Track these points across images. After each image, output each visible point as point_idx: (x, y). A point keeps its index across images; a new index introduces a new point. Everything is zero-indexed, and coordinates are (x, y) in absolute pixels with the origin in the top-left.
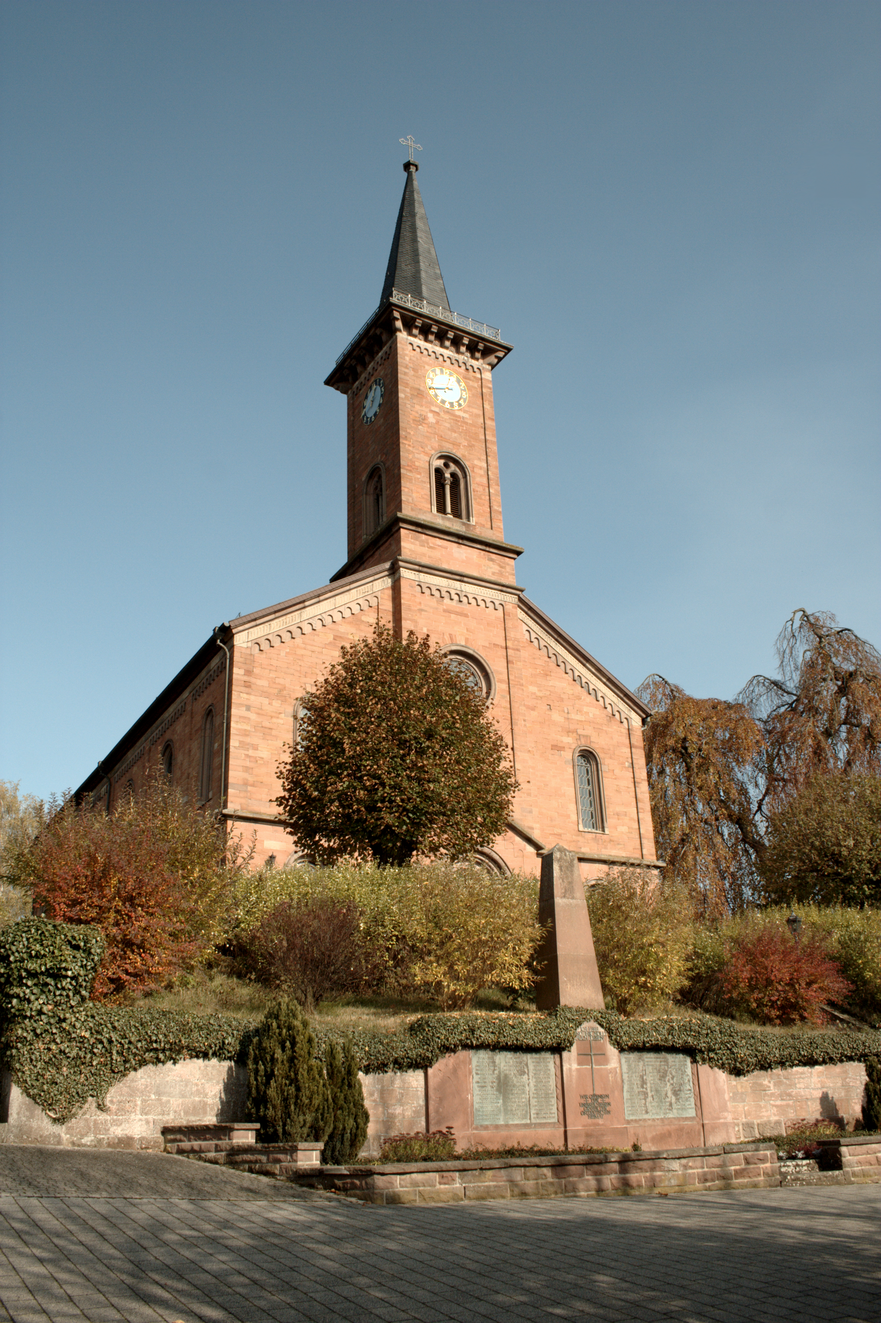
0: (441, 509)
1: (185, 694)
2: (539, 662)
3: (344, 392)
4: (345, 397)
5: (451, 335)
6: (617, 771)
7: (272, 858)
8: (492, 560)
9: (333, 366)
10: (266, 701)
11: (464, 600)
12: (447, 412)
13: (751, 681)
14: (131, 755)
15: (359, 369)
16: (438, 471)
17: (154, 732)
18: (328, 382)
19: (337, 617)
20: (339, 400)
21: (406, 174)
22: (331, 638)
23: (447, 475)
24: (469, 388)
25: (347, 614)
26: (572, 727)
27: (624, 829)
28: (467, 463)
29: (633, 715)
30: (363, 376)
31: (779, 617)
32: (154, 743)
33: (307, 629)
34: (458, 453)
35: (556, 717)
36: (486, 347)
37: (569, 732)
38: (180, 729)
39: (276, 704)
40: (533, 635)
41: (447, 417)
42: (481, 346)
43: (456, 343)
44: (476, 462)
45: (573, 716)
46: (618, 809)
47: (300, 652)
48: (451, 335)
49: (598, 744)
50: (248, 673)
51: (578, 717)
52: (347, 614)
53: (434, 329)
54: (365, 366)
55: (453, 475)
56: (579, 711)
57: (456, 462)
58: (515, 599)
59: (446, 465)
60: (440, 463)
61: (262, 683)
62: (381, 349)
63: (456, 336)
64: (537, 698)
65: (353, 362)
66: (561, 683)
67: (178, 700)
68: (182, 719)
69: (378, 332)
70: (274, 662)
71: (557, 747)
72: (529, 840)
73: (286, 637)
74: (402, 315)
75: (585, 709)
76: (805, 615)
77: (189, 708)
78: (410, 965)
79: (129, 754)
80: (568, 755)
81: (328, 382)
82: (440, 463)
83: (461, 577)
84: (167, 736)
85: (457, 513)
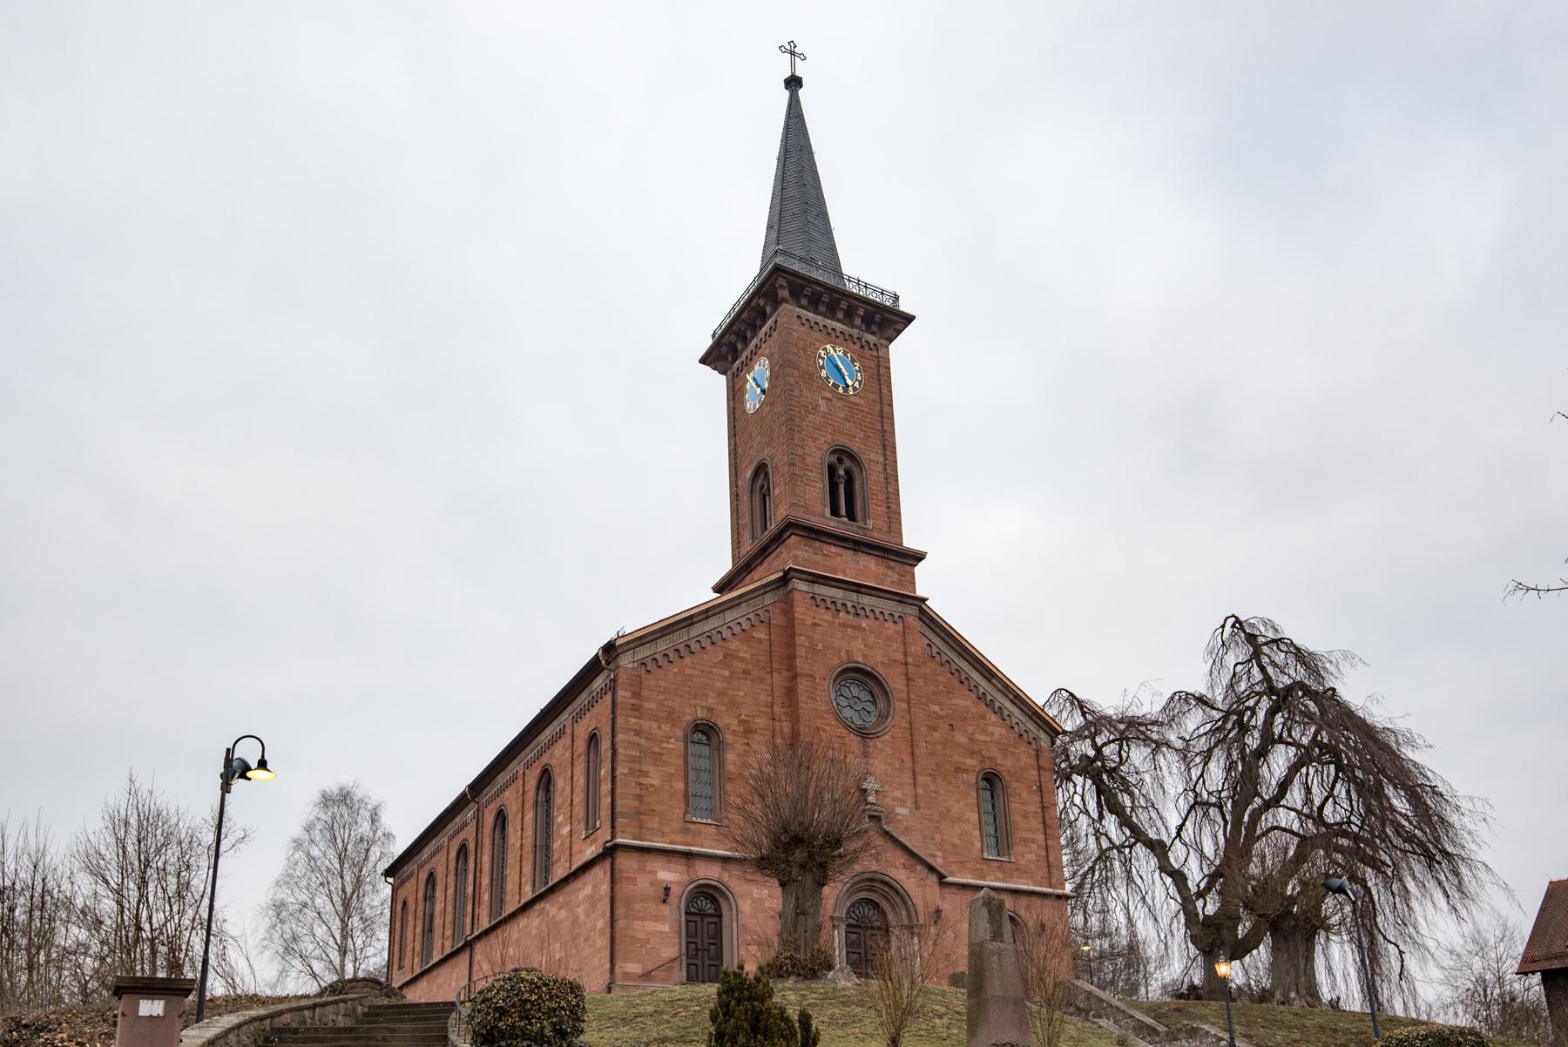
0: (835, 512)
1: (564, 716)
2: (940, 678)
3: (723, 372)
4: (724, 378)
5: (844, 305)
6: (1024, 795)
7: (667, 889)
8: (890, 568)
9: (709, 342)
10: (655, 725)
11: (862, 613)
12: (840, 398)
13: (1172, 698)
14: (501, 779)
15: (739, 346)
16: (832, 470)
17: (527, 754)
18: (703, 361)
19: (726, 633)
20: (717, 383)
21: (787, 93)
22: (721, 657)
23: (842, 472)
24: (864, 368)
25: (737, 630)
26: (976, 748)
27: (1032, 857)
28: (863, 458)
29: (1043, 735)
30: (745, 354)
31: (1205, 627)
32: (528, 766)
33: (695, 647)
34: (855, 446)
35: (960, 738)
36: (883, 319)
37: (972, 754)
38: (558, 755)
39: (666, 728)
40: (935, 650)
41: (840, 404)
42: (878, 318)
43: (849, 314)
44: (872, 456)
45: (978, 737)
46: (1025, 835)
47: (688, 671)
48: (844, 305)
49: (1005, 764)
50: (636, 695)
51: (983, 738)
52: (737, 630)
53: (826, 299)
54: (746, 341)
55: (848, 472)
56: (984, 731)
57: (851, 456)
58: (915, 611)
59: (840, 461)
60: (834, 459)
61: (651, 705)
62: (764, 323)
63: (849, 307)
64: (939, 717)
65: (733, 338)
66: (965, 702)
67: (556, 723)
68: (561, 743)
69: (762, 302)
70: (662, 684)
71: (959, 770)
72: (931, 869)
73: (672, 656)
74: (789, 283)
75: (991, 729)
76: (1237, 620)
77: (568, 730)
78: (768, 1003)
79: (499, 778)
80: (972, 778)
81: (703, 361)
82: (834, 459)
83: (858, 588)
84: (545, 759)
85: (851, 516)
